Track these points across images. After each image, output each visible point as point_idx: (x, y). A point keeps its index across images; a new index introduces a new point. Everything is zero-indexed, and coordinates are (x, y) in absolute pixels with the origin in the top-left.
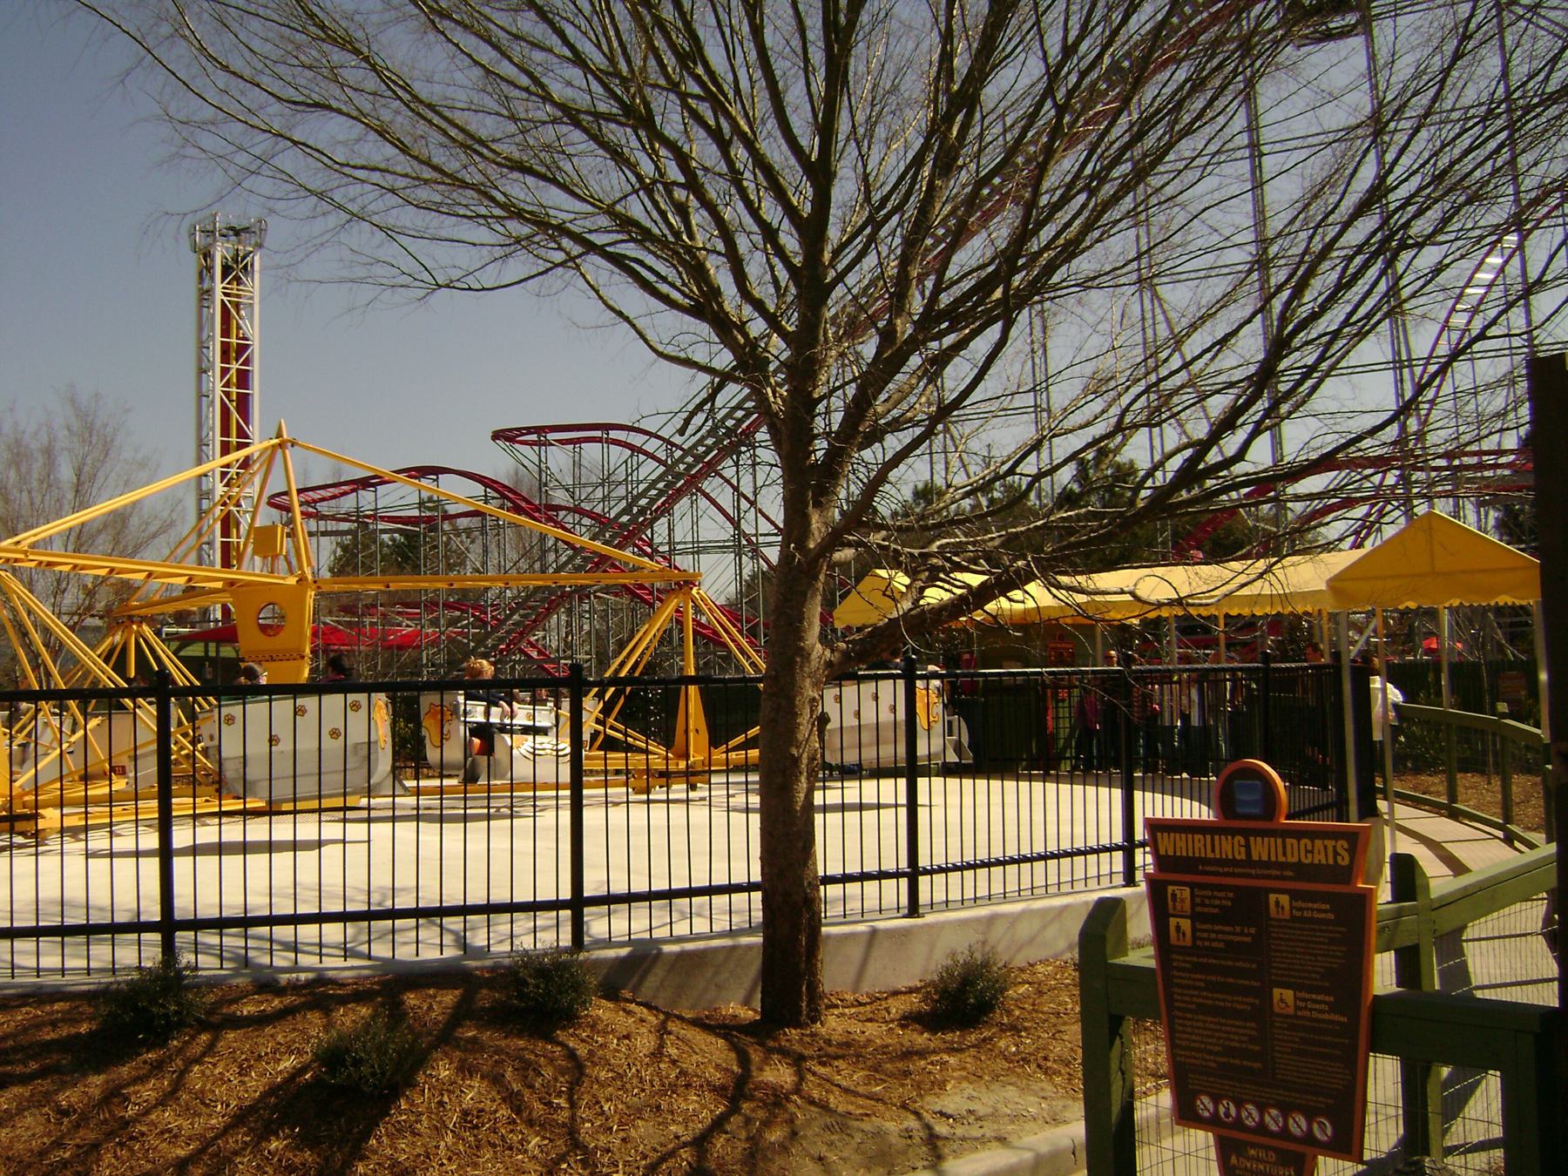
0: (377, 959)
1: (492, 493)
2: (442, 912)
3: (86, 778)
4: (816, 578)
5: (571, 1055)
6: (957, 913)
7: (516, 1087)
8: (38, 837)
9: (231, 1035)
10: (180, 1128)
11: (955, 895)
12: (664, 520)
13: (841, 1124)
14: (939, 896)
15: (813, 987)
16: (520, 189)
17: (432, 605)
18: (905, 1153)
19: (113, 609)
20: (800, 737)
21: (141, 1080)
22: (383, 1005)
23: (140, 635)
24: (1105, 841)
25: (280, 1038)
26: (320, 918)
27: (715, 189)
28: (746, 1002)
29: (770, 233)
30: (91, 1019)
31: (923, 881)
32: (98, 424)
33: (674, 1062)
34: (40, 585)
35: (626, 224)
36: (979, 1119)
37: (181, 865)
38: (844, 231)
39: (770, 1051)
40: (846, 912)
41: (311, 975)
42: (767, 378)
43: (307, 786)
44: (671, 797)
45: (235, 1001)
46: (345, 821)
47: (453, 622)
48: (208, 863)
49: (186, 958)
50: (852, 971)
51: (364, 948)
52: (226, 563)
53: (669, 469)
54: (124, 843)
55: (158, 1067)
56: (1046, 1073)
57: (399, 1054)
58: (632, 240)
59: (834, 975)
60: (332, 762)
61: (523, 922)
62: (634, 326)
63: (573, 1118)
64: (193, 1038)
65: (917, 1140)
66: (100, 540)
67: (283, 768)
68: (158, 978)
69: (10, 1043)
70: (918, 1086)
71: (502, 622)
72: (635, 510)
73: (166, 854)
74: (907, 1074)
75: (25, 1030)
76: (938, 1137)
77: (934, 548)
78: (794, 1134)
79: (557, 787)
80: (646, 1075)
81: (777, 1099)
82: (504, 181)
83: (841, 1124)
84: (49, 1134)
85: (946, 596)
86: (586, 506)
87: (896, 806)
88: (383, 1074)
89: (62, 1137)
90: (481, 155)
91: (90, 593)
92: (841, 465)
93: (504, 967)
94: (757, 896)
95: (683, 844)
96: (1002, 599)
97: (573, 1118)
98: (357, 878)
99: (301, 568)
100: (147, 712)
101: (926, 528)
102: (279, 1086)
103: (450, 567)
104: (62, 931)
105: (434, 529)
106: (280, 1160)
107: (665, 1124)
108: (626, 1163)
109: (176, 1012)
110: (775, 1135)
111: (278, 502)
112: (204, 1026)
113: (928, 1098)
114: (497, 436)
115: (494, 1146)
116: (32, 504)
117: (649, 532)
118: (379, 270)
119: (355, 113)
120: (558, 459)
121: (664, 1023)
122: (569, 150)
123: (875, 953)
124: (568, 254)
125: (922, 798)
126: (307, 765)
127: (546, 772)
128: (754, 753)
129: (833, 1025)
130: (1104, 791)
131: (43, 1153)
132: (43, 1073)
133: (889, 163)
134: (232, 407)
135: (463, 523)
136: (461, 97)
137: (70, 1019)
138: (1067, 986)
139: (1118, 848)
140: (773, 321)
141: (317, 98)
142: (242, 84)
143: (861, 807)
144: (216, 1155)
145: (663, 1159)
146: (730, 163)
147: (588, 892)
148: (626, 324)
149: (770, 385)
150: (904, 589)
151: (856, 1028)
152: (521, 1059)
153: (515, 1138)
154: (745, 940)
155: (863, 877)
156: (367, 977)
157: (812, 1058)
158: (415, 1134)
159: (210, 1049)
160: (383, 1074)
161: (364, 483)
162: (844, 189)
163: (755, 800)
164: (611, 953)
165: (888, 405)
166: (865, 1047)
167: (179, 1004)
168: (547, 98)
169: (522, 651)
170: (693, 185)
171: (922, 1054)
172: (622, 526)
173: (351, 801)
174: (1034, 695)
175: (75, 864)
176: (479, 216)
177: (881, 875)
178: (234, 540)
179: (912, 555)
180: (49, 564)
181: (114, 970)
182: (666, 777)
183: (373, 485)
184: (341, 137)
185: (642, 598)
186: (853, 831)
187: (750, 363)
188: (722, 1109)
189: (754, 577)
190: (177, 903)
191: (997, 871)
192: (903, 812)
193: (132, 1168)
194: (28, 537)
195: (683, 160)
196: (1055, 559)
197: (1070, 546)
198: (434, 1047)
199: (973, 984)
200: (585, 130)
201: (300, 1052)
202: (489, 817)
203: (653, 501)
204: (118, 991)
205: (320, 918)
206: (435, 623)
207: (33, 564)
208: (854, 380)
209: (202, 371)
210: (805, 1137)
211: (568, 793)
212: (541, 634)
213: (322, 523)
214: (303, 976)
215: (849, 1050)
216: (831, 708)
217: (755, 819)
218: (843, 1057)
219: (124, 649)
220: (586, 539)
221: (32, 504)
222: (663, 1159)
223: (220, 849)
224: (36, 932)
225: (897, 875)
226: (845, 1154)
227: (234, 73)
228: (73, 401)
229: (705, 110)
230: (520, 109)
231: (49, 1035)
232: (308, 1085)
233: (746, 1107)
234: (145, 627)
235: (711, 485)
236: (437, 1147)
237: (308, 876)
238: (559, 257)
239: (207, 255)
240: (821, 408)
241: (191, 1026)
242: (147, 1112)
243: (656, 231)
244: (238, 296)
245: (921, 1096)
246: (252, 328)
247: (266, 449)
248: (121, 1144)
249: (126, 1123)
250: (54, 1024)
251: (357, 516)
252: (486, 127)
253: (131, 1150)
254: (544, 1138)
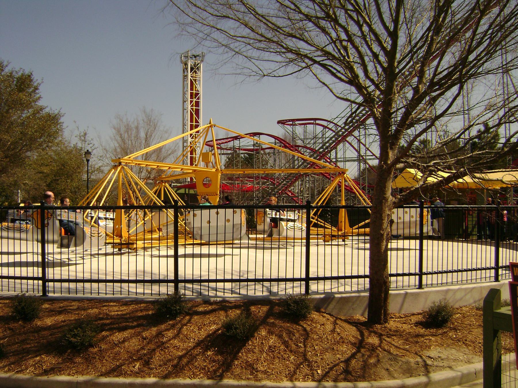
0: (242, 295)
1: (277, 141)
2: (263, 280)
3: (151, 232)
4: (390, 173)
5: (305, 330)
6: (436, 290)
7: (286, 339)
8: (136, 250)
9: (196, 317)
10: (180, 346)
11: (435, 282)
12: (334, 151)
13: (395, 358)
14: (429, 282)
15: (386, 311)
16: (291, 43)
17: (257, 178)
18: (416, 369)
19: (156, 178)
20: (384, 227)
21: (168, 330)
22: (244, 310)
23: (165, 186)
24: (488, 266)
25: (211, 319)
26: (224, 281)
27: (358, 41)
28: (362, 315)
29: (375, 56)
30: (152, 310)
31: (424, 277)
32: (152, 119)
33: (339, 334)
34: (134, 169)
35: (327, 54)
36: (442, 360)
37: (181, 261)
38: (401, 55)
39: (371, 332)
40: (397, 286)
41: (221, 299)
42: (374, 106)
43: (221, 237)
44: (333, 243)
45: (197, 306)
46: (233, 248)
47: (264, 183)
48: (189, 260)
49: (182, 291)
50: (399, 306)
51: (238, 291)
52: (192, 164)
53: (337, 134)
54: (163, 252)
55: (173, 326)
56: (466, 345)
57: (249, 326)
58: (329, 59)
59: (393, 307)
60: (229, 229)
61: (289, 284)
62: (328, 87)
63: (305, 350)
64: (184, 317)
65: (420, 365)
66: (153, 156)
67: (213, 231)
68: (174, 298)
69: (128, 316)
70: (421, 347)
71: (280, 184)
72: (324, 147)
73: (176, 257)
74: (417, 342)
75: (133, 312)
76: (428, 365)
77: (432, 163)
78: (379, 360)
79: (302, 239)
80: (329, 337)
81: (373, 349)
82: (286, 40)
83: (395, 358)
84: (140, 345)
85: (435, 180)
86: (308, 146)
87: (416, 249)
88: (244, 333)
89: (144, 346)
90: (279, 32)
91: (149, 173)
92: (400, 135)
93: (283, 299)
94: (367, 280)
95: (343, 260)
96: (455, 182)
97: (305, 350)
98: (236, 267)
99: (217, 166)
100: (171, 211)
101: (429, 157)
102: (211, 335)
103: (263, 165)
104: (144, 281)
105: (258, 153)
106: (211, 358)
107: (335, 354)
108: (322, 367)
109: (179, 309)
110: (372, 361)
111: (209, 144)
112: (187, 314)
113: (424, 351)
114: (279, 122)
115: (279, 358)
116: (132, 144)
117: (329, 155)
118: (245, 71)
119: (237, 19)
120: (299, 130)
121: (335, 321)
122: (307, 29)
123: (407, 300)
124: (307, 64)
125: (425, 247)
126: (221, 230)
127: (298, 234)
128: (368, 230)
129: (392, 324)
130: (488, 247)
131: (138, 351)
132: (138, 326)
133: (419, 30)
134: (194, 113)
135: (267, 151)
136: (272, 12)
137: (146, 309)
138: (474, 315)
139: (493, 268)
140: (377, 86)
141: (224, 14)
142: (201, 11)
143: (403, 249)
144: (191, 355)
145: (335, 366)
146: (362, 32)
147: (311, 276)
148: (326, 87)
149: (375, 108)
150: (420, 178)
151: (400, 325)
152: (288, 330)
153: (286, 356)
154: (363, 294)
155: (403, 275)
156: (239, 301)
157: (385, 335)
158: (253, 352)
159: (189, 321)
160: (244, 333)
161: (236, 138)
162: (402, 40)
163: (368, 246)
164: (318, 296)
165: (416, 115)
166: (403, 332)
167: (180, 307)
168: (300, 12)
169: (286, 193)
170: (350, 40)
171: (422, 336)
172: (320, 152)
173: (235, 242)
174: (462, 214)
175: (148, 259)
176: (277, 52)
177: (410, 274)
178: (194, 156)
179: (424, 166)
180: (139, 164)
181: (159, 294)
182: (333, 237)
183: (239, 139)
184: (232, 27)
185: (328, 177)
186: (401, 258)
187: (369, 100)
188: (354, 350)
189: (364, 170)
190: (179, 273)
191: (450, 274)
192: (418, 252)
193: (165, 357)
194: (133, 156)
195: (346, 31)
196: (475, 168)
197: (480, 164)
198: (260, 325)
199: (441, 313)
200: (313, 23)
201: (217, 324)
202: (279, 248)
203: (331, 144)
204: (161, 301)
205: (224, 281)
206: (258, 183)
207: (134, 164)
208: (404, 107)
209: (184, 102)
210: (382, 362)
211: (305, 241)
212: (293, 188)
213: (222, 151)
214: (218, 299)
215: (397, 333)
216: (394, 217)
217: (368, 252)
218: (395, 335)
219: (160, 190)
220: (308, 157)
221: (132, 144)
222: (335, 366)
223: (193, 256)
224: (136, 281)
225: (415, 274)
226: (396, 368)
227: (198, 7)
228: (145, 112)
229: (354, 15)
230: (291, 16)
231: (140, 314)
232: (220, 335)
233: (363, 350)
234: (167, 184)
235: (349, 139)
236: (261, 357)
237: (220, 266)
238: (304, 65)
239: (186, 64)
240: (393, 116)
241: (183, 314)
242: (170, 340)
243: (337, 56)
244: (196, 77)
245: (422, 350)
246: (200, 88)
247: (206, 128)
248: (162, 350)
249: (163, 343)
250: (141, 311)
251: (233, 149)
252: (280, 23)
253: (165, 352)
254: (295, 356)
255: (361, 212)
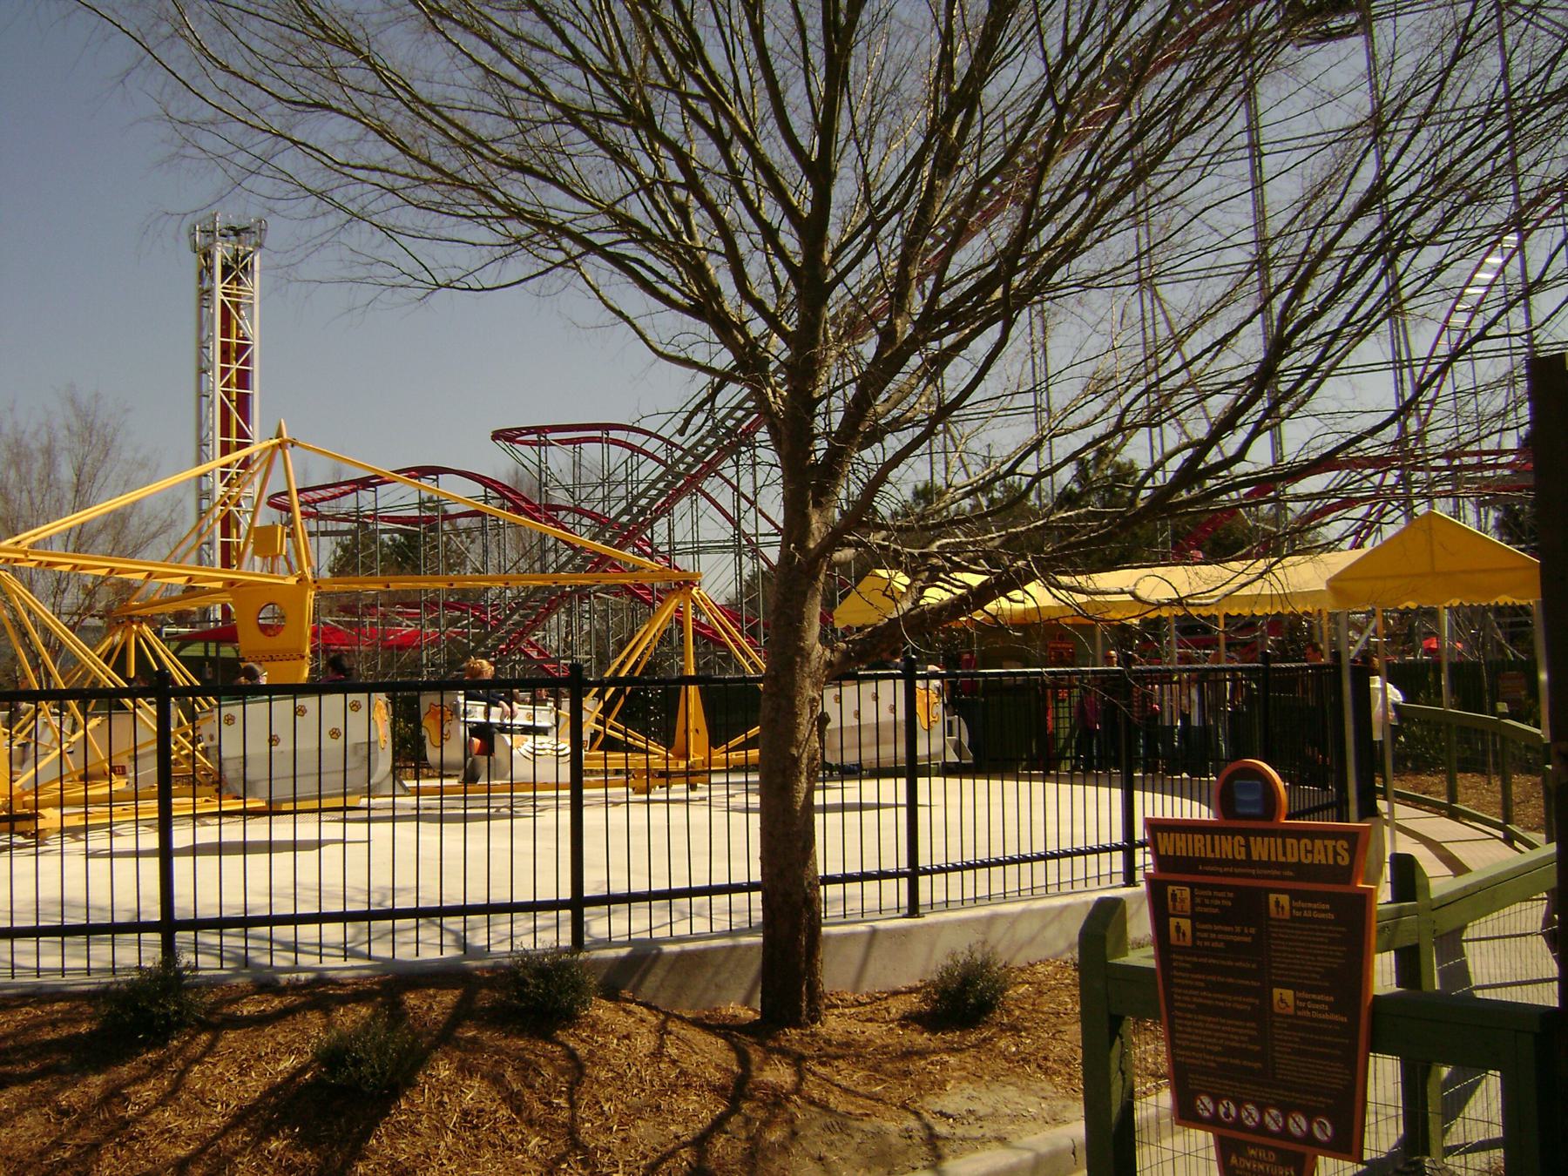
0: (377, 959)
1: (492, 493)
2: (442, 912)
3: (86, 778)
4: (816, 578)
5: (571, 1055)
7: (516, 1087)
8: (38, 837)
9: (231, 1035)
10: (180, 1128)
11: (955, 895)
12: (664, 520)
13: (841, 1124)
14: (939, 896)
15: (813, 987)
16: (520, 189)
17: (432, 605)
18: (905, 1153)
19: (113, 609)
20: (800, 737)
21: (141, 1080)
22: (383, 1005)
23: (140, 635)
24: (1105, 841)
25: (280, 1038)
26: (320, 918)
27: (715, 189)
28: (746, 1002)
29: (770, 233)
30: (91, 1019)
31: (923, 881)
32: (98, 424)
33: (674, 1062)
34: (40, 585)
35: (626, 224)
36: (979, 1119)
37: (181, 865)
38: (844, 231)
39: (770, 1051)
40: (846, 912)
41: (311, 975)
42: (767, 378)
43: (307, 786)
44: (671, 797)
45: (235, 1001)
46: (345, 821)
47: (453, 622)
48: (208, 863)
49: (186, 958)
50: (852, 971)
51: (364, 948)
52: (226, 563)
53: (669, 469)
54: (124, 843)
55: (158, 1067)
56: (1046, 1073)
57: (399, 1054)
58: (632, 240)
59: (834, 975)
60: (332, 762)
61: (523, 922)
62: (634, 326)
63: (573, 1118)
64: (193, 1038)
65: (917, 1140)
66: (100, 540)
67: (283, 768)
68: (158, 978)
69: (10, 1043)
70: (918, 1086)
71: (502, 622)
72: (635, 510)
73: (166, 854)
74: (907, 1074)
75: (25, 1030)
76: (938, 1137)
77: (934, 548)
78: (794, 1134)
79: (557, 787)
80: (646, 1075)
81: (777, 1099)
82: (504, 181)
83: (841, 1124)
84: (49, 1134)
85: (946, 596)
86: (586, 506)
87: (896, 806)
88: (383, 1074)
89: (62, 1137)
90: (481, 155)
91: (90, 593)
92: (841, 465)
93: (504, 967)
94: (757, 896)
95: (683, 844)
96: (1002, 599)
97: (573, 1118)
98: (357, 878)
99: (301, 568)
100: (147, 712)
101: (926, 528)
102: (279, 1086)
103: (450, 567)
104: (62, 931)
105: (434, 529)
106: (280, 1160)
107: (665, 1124)
108: (626, 1163)
109: (176, 1012)
110: (775, 1135)
111: (278, 502)
112: (204, 1026)
113: (928, 1098)
114: (497, 436)
115: (494, 1146)
116: (32, 504)
117: (649, 532)
118: (379, 270)
119: (355, 113)
120: (558, 459)
121: (664, 1023)
122: (569, 150)
123: (875, 953)
124: (568, 254)
125: (922, 798)
126: (307, 765)
127: (546, 772)
128: (754, 753)
129: (833, 1025)
130: (1104, 791)
131: (43, 1153)
132: (43, 1073)
133: (889, 163)
134: (232, 407)
135: (463, 523)
136: (461, 97)
137: (70, 1019)
138: (1067, 986)
139: (1118, 848)
140: (773, 321)
141: (317, 98)
142: (242, 84)
143: (861, 807)
144: (216, 1155)
145: (663, 1159)
146: (730, 163)
147: (588, 892)
148: (626, 324)
149: (770, 385)
150: (904, 589)
151: (856, 1028)
152: (521, 1059)
153: (515, 1138)
154: (745, 940)
155: (863, 877)
156: (367, 977)
157: (812, 1058)
158: (415, 1134)
159: (210, 1049)
160: (383, 1074)
161: (364, 483)
162: (844, 189)
163: (755, 800)
164: (611, 953)
165: (888, 405)
166: (865, 1047)
167: (179, 1004)
168: (547, 98)
169: (522, 651)
170: (693, 185)
171: (922, 1054)
172: (622, 526)
173: (351, 801)
175: (75, 864)
176: (479, 216)
177: (881, 875)
178: (234, 540)
179: (912, 555)
180: (49, 564)
181: (114, 970)
182: (666, 777)
183: (373, 485)
184: (341, 137)
185: (642, 598)
186: (853, 831)
187: (750, 363)
188: (722, 1109)
189: (754, 577)
190: (177, 903)
191: (997, 871)
192: (903, 812)
193: (132, 1168)
194: (28, 537)
195: (683, 160)
196: (1055, 559)
197: (1070, 546)
198: (434, 1047)
199: (973, 984)
200: (585, 130)
201: (300, 1052)
202: (489, 817)
203: (653, 501)
204: (118, 991)
205: (320, 918)
206: (435, 623)
207: (33, 564)
208: (854, 380)
209: (202, 371)
210: (805, 1137)
211: (568, 793)
212: (541, 634)
213: (322, 523)
214: (303, 976)
215: (849, 1050)
216: (831, 708)
217: (755, 819)
218: (843, 1057)
219: (124, 649)
220: (586, 539)
221: (32, 504)
222: (663, 1159)
223: (220, 849)
224: (36, 932)
225: (897, 875)
226: (845, 1154)
227: (234, 73)
228: (73, 401)
229: (705, 110)
230: (520, 109)
231: (49, 1035)
232: (308, 1085)
233: (746, 1107)
234: (145, 627)
235: (711, 485)
236: (437, 1147)
237: (308, 876)
238: (559, 257)
239: (207, 255)
240: (821, 408)
241: (191, 1026)
242: (147, 1112)
243: (656, 231)
244: (238, 296)
245: (921, 1096)
246: (252, 328)
247: (266, 449)
248: (121, 1144)
249: (126, 1123)
250: (54, 1024)
251: (357, 516)
252: (486, 127)
253: (131, 1150)
254: (544, 1138)
255: (739, 704)
